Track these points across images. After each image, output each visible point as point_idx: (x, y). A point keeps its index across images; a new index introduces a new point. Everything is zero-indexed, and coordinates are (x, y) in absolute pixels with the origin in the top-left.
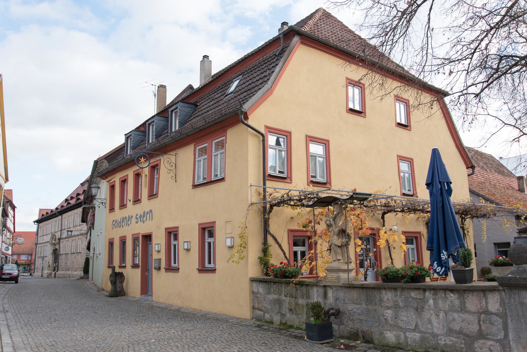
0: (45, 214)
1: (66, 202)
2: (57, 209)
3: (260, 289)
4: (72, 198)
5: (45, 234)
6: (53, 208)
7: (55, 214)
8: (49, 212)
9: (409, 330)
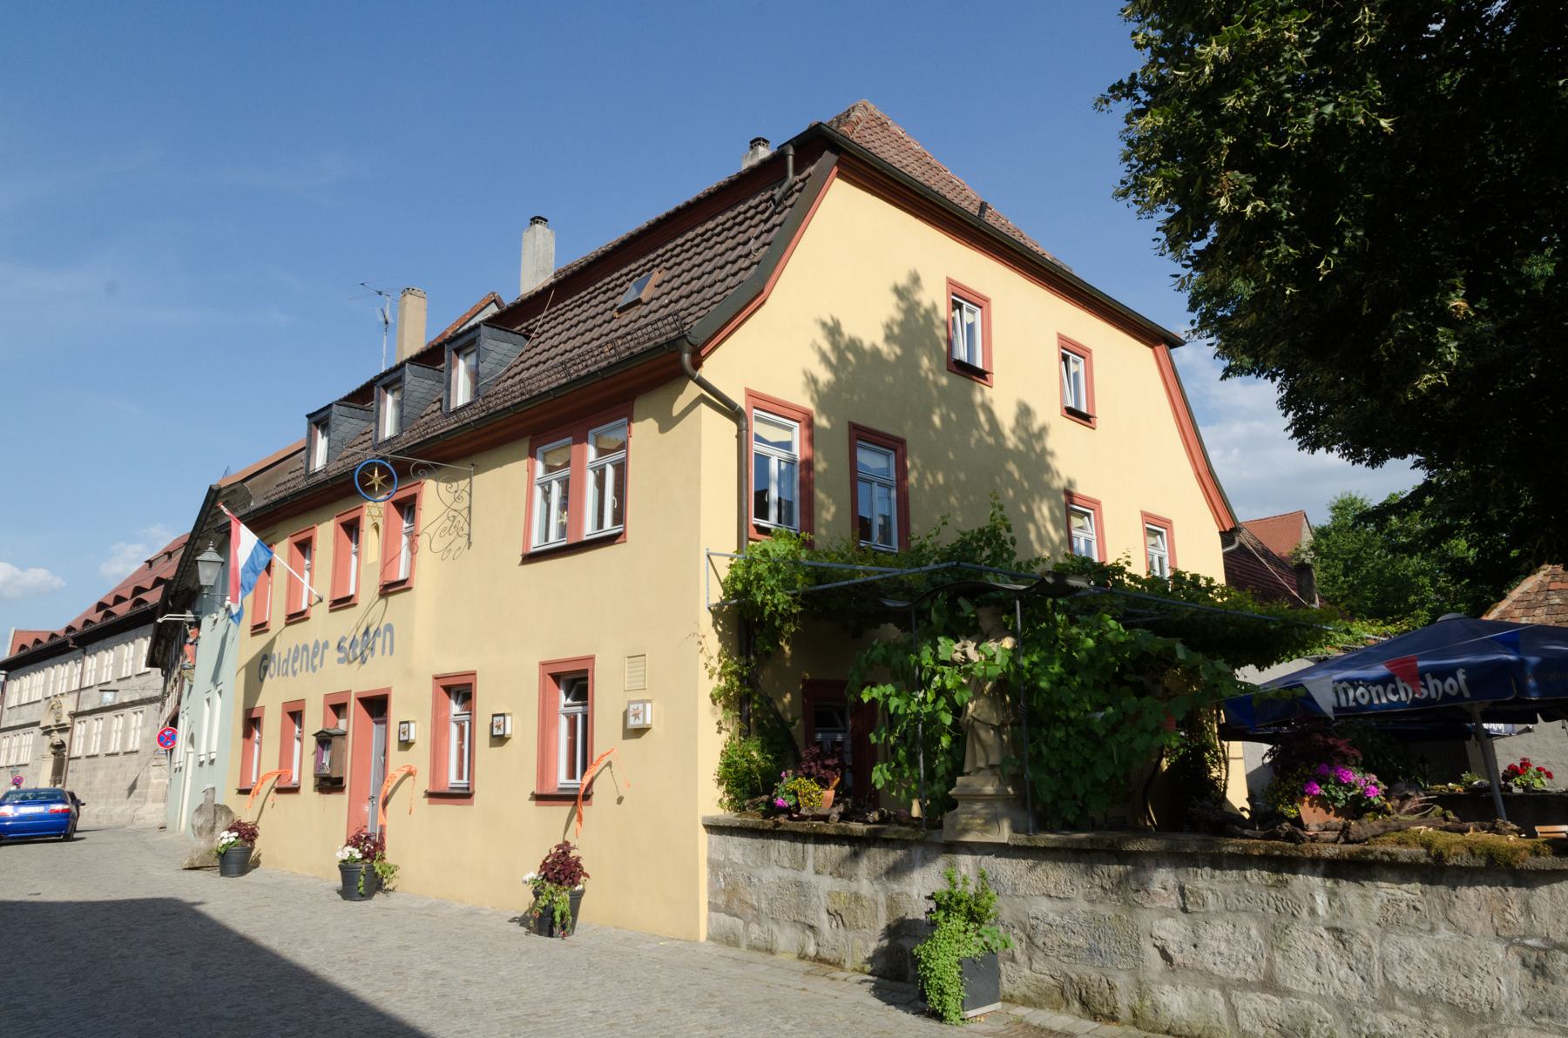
0: (30, 645)
1: (98, 610)
2: (70, 629)
3: (732, 849)
4: (119, 600)
5: (24, 701)
6: (59, 627)
7: (65, 643)
8: (45, 640)
9: (1244, 985)
